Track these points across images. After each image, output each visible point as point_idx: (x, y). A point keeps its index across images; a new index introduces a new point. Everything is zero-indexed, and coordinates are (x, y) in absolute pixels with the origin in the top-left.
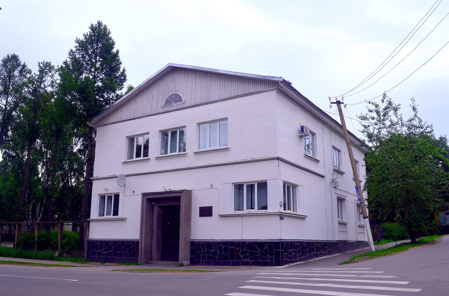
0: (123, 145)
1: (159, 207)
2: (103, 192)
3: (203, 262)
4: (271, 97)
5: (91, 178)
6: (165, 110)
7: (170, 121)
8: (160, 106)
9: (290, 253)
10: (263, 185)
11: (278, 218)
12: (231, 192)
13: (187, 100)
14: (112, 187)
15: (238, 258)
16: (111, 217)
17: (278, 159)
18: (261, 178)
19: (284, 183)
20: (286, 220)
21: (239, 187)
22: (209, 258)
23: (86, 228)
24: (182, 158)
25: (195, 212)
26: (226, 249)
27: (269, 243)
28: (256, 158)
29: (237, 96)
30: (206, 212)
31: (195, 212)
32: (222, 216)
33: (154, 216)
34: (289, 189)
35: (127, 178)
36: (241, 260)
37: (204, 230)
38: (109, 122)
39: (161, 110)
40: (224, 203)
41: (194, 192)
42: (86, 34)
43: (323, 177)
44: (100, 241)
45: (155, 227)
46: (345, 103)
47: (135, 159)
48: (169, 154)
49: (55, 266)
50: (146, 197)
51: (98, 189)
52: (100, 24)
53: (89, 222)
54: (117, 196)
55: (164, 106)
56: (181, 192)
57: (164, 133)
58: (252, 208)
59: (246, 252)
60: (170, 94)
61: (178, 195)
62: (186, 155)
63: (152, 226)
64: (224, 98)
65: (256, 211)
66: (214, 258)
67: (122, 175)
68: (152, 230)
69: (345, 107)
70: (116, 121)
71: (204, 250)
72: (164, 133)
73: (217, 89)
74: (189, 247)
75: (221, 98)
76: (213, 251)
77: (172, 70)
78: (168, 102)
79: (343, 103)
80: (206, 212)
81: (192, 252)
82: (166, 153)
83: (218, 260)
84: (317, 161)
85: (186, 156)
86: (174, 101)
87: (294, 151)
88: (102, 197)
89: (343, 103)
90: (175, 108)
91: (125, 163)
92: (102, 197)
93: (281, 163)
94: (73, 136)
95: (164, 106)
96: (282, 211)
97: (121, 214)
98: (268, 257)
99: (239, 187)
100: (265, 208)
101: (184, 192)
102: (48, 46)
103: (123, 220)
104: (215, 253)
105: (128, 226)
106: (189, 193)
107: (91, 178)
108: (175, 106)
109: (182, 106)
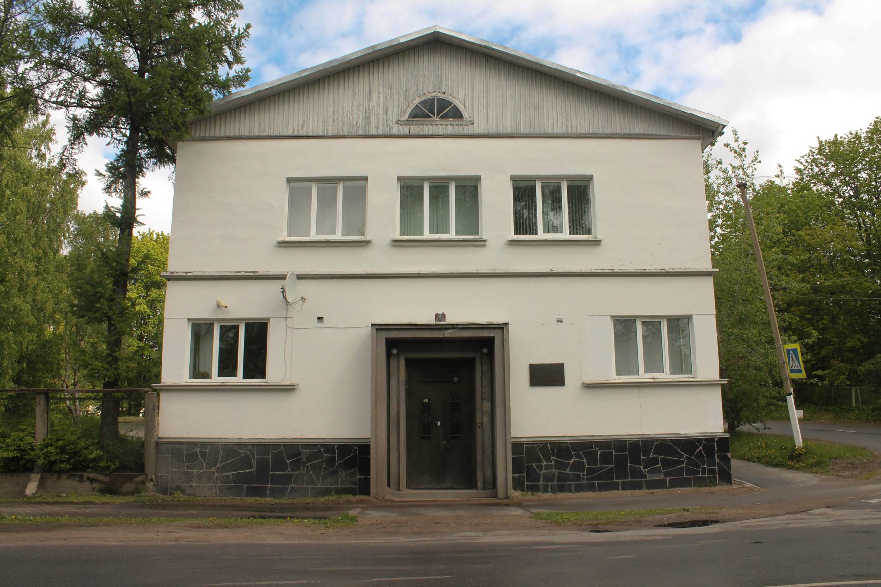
2: (204, 313)
6: (405, 130)
7: (437, 156)
15: (638, 474)
18: (255, 313)
21: (624, 326)
22: (608, 474)
23: (154, 409)
26: (606, 458)
27: (706, 440)
28: (669, 267)
29: (624, 134)
30: (547, 376)
37: (534, 416)
40: (592, 356)
41: (513, 332)
44: (212, 444)
48: (541, 235)
49: (865, 519)
59: (655, 461)
65: (238, 379)
66: (578, 477)
71: (548, 459)
72: (410, 189)
76: (572, 461)
77: (436, 44)
80: (547, 376)
81: (517, 466)
83: (588, 480)
86: (437, 111)
88: (200, 331)
91: (284, 244)
94: (158, 147)
95: (407, 123)
97: (275, 372)
98: (704, 469)
99: (624, 326)
100: (262, 374)
104: (578, 466)
108: (442, 126)
109: (459, 130)
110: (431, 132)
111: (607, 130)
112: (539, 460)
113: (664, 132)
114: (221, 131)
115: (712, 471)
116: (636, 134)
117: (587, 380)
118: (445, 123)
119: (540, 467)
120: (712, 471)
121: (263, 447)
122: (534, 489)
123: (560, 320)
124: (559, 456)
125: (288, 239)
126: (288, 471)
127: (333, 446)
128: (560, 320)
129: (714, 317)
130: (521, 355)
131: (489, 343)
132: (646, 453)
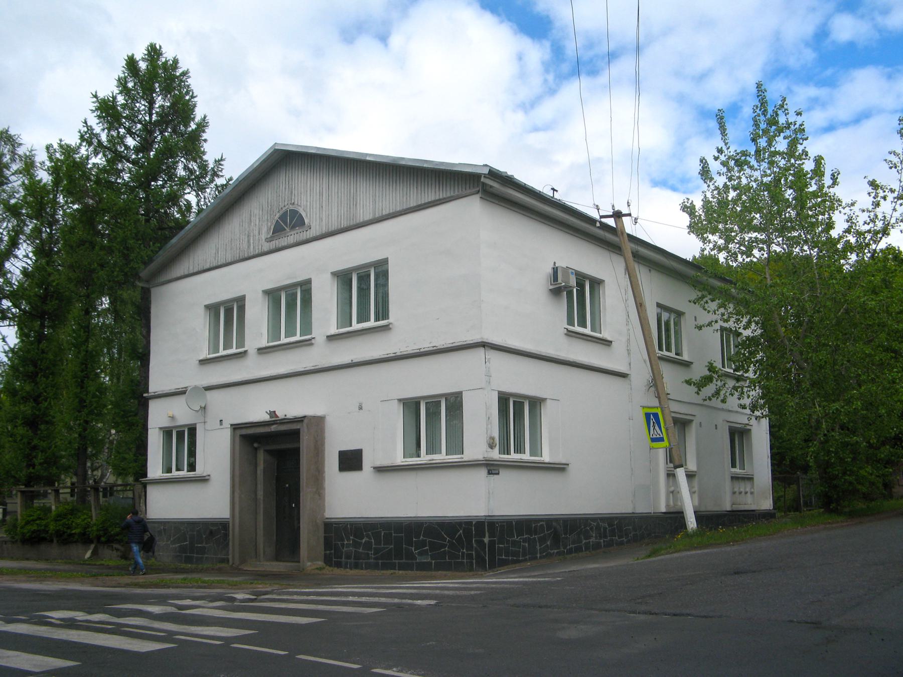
0: (200, 323)
1: (266, 451)
2: (166, 423)
3: (346, 564)
4: (471, 210)
5: (145, 395)
8: (263, 237)
9: (514, 543)
10: (455, 403)
11: (483, 472)
12: (397, 418)
13: (315, 222)
14: (178, 412)
15: (411, 556)
16: (184, 473)
17: (484, 346)
19: (503, 399)
20: (503, 473)
21: (411, 406)
23: (140, 497)
25: (332, 462)
30: (351, 461)
31: (332, 462)
32: (380, 470)
33: (259, 472)
34: (516, 411)
35: (208, 393)
36: (414, 558)
37: (348, 498)
39: (266, 247)
40: (386, 442)
43: (623, 376)
45: (260, 494)
46: (634, 215)
47: (356, 326)
50: (239, 432)
51: (158, 416)
52: (154, 52)
53: (145, 486)
54: (192, 430)
55: (269, 240)
56: (300, 420)
57: (343, 278)
59: (423, 544)
60: (281, 212)
62: (313, 341)
63: (255, 492)
64: (383, 216)
66: (368, 557)
68: (256, 500)
69: (636, 221)
70: (186, 273)
71: (348, 540)
73: (370, 197)
74: (321, 534)
75: (377, 215)
78: (278, 230)
79: (629, 215)
80: (351, 461)
81: (328, 543)
83: (375, 559)
84: (607, 343)
85: (312, 344)
86: (289, 225)
87: (542, 325)
88: (167, 433)
89: (629, 215)
90: (291, 239)
91: (203, 362)
92: (167, 433)
93: (493, 355)
96: (495, 454)
97: (200, 470)
98: (463, 553)
99: (411, 406)
101: (306, 421)
102: (57, 113)
103: (204, 480)
104: (368, 546)
105: (196, 493)
106: (318, 422)
107: (145, 395)
110: (305, 238)
111: (413, 204)
112: (343, 540)
113: (441, 195)
114: (163, 279)
115: (470, 556)
116: (425, 204)
117: (378, 464)
118: (295, 232)
119: (343, 545)
120: (470, 556)
121: (193, 524)
122: (339, 565)
123: (361, 408)
124: (355, 536)
125: (268, 345)
126: (204, 545)
127: (511, 522)
128: (361, 408)
129: (149, 427)
130: (338, 440)
131: (295, 435)
132: (418, 536)
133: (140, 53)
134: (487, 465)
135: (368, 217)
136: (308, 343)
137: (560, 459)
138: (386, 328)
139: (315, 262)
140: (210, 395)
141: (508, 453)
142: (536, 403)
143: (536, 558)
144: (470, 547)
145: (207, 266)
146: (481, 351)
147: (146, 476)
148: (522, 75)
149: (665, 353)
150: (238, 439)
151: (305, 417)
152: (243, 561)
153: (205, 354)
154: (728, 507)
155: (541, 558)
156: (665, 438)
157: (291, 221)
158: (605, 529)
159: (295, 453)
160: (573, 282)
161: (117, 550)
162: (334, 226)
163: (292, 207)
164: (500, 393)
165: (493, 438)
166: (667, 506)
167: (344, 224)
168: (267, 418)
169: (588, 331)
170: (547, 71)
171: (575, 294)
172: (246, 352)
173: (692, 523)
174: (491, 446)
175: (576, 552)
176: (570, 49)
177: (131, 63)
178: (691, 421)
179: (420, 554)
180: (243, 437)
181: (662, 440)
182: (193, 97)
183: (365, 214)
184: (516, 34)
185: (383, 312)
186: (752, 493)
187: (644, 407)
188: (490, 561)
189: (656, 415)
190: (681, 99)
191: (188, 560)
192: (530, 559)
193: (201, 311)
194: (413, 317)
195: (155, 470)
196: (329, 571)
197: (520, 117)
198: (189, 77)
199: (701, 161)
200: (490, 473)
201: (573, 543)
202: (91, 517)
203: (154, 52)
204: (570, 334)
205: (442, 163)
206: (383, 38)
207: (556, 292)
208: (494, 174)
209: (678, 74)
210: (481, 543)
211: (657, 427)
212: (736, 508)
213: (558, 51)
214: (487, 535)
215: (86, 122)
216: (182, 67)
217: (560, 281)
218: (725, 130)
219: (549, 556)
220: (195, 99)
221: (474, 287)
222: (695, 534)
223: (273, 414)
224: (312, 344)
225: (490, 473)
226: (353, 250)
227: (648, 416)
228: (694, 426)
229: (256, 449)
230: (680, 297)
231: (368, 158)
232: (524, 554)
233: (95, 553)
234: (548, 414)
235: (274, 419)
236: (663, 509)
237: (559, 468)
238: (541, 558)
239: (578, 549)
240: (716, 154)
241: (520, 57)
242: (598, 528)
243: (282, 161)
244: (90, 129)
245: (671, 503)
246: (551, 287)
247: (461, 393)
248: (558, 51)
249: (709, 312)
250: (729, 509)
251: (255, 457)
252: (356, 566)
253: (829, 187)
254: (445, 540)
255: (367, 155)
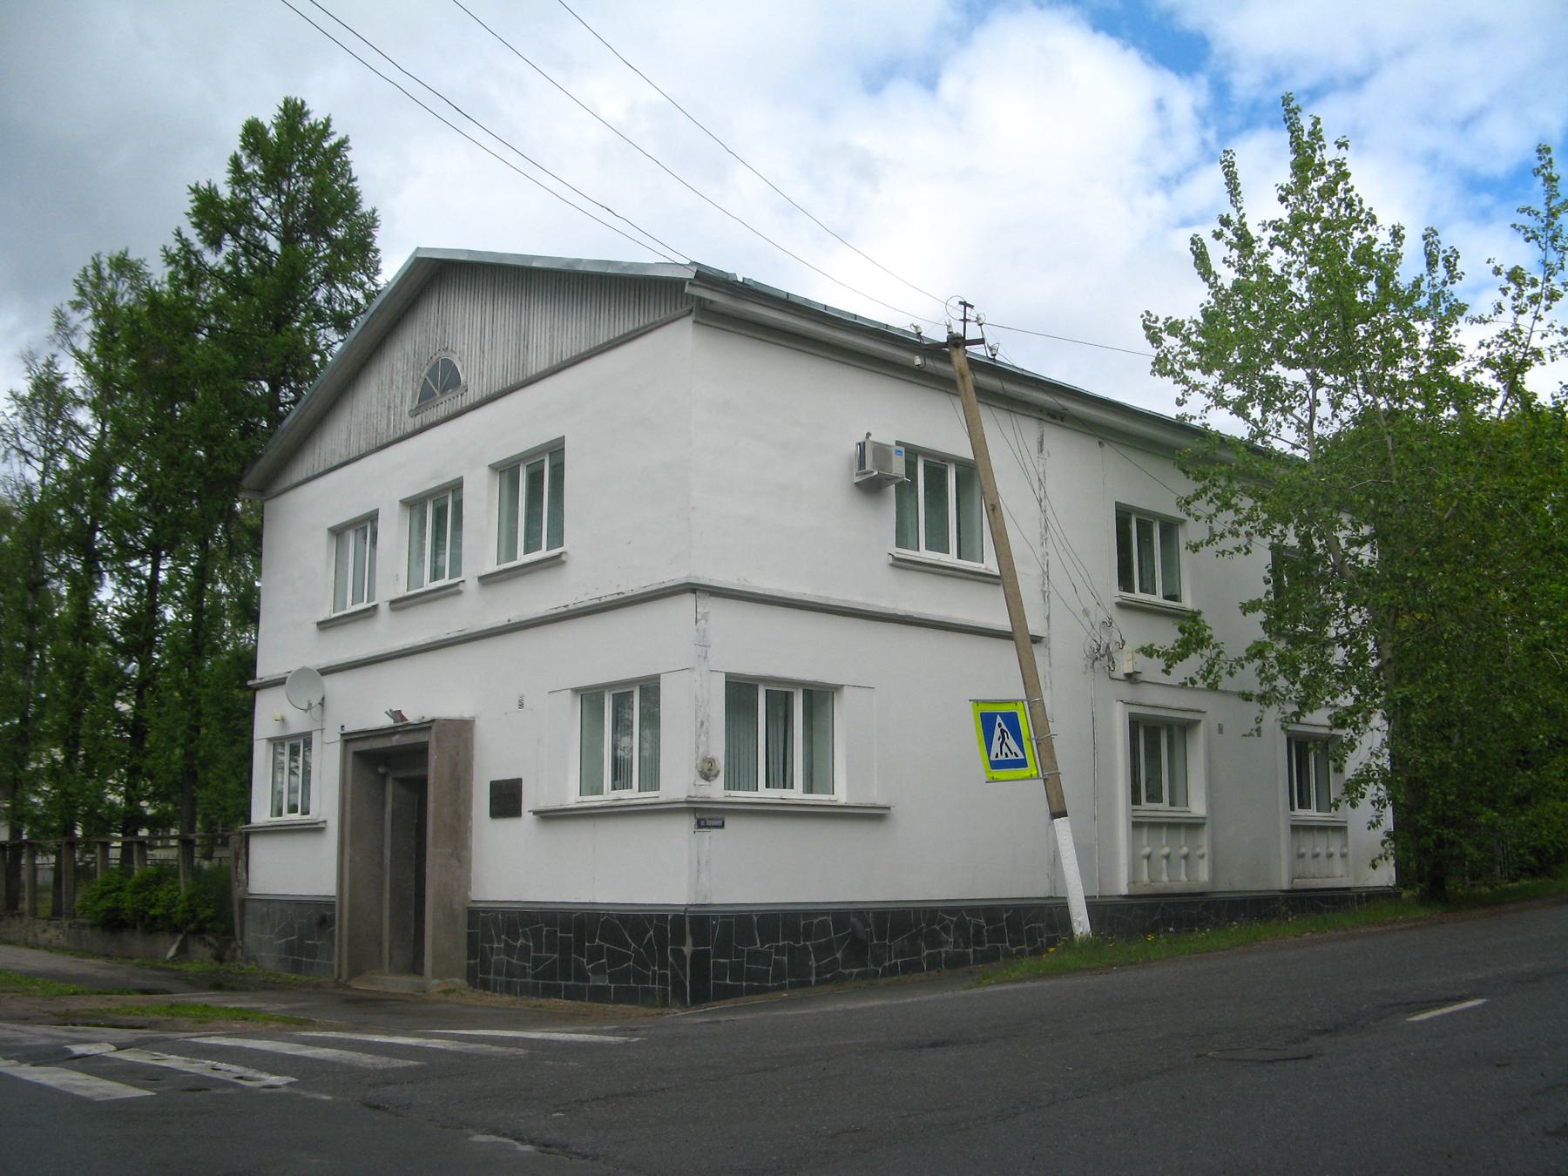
1: (395, 779)
2: (275, 732)
4: (680, 349)
5: (250, 683)
9: (754, 957)
11: (686, 824)
15: (581, 975)
21: (590, 697)
24: (451, 600)
32: (547, 816)
36: (587, 979)
37: (513, 867)
38: (287, 484)
39: (410, 424)
42: (175, 247)
52: (293, 112)
53: (246, 837)
55: (414, 413)
56: (425, 726)
58: (787, 783)
61: (420, 738)
62: (461, 587)
67: (304, 671)
68: (381, 865)
71: (499, 941)
73: (549, 330)
78: (426, 397)
80: (506, 799)
81: (474, 946)
82: (512, 556)
85: (460, 593)
86: (441, 390)
87: (853, 552)
89: (982, 341)
90: (441, 411)
91: (324, 626)
92: (276, 742)
96: (716, 790)
106: (460, 731)
107: (250, 683)
111: (603, 338)
112: (491, 942)
113: (645, 321)
115: (663, 978)
122: (485, 985)
123: (521, 705)
128: (521, 705)
130: (490, 767)
133: (268, 116)
134: (694, 811)
135: (543, 366)
136: (452, 591)
137: (873, 796)
138: (556, 562)
139: (467, 448)
140: (331, 682)
141: (599, 791)
142: (819, 697)
143: (807, 984)
144: (664, 965)
145: (335, 463)
146: (688, 600)
147: (249, 822)
148: (1166, 134)
149: (1138, 595)
150: (350, 757)
151: (433, 721)
152: (356, 970)
153: (326, 613)
154: (1282, 881)
155: (818, 983)
156: (1030, 761)
157: (443, 378)
158: (979, 928)
159: (418, 787)
160: (898, 467)
161: (210, 945)
162: (497, 388)
163: (444, 355)
164: (728, 675)
165: (711, 762)
166: (1133, 882)
167: (511, 381)
168: (388, 722)
169: (950, 559)
170: (1205, 125)
171: (927, 496)
172: (375, 607)
173: (1081, 923)
174: (707, 775)
175: (904, 972)
176: (1245, 84)
177: (253, 131)
178: (1198, 722)
179: (595, 971)
180: (360, 755)
181: (1022, 764)
182: (351, 180)
183: (538, 363)
184: (1148, 63)
185: (557, 537)
186: (1344, 856)
187: (977, 701)
188: (702, 989)
189: (1011, 720)
190: (1432, 160)
191: (296, 967)
192: (792, 986)
193: (323, 538)
194: (604, 542)
195: (261, 814)
196: (477, 998)
197: (1159, 202)
198: (348, 149)
199: (1193, 242)
200: (701, 825)
201: (901, 954)
202: (178, 889)
203: (293, 112)
204: (899, 564)
205: (631, 265)
206: (930, 83)
207: (871, 487)
208: (706, 277)
209: (1427, 119)
210: (678, 954)
211: (1011, 741)
212: (1300, 884)
213: (1221, 89)
214: (689, 940)
215: (179, 234)
216: (338, 132)
217: (868, 467)
218: (1237, 186)
219: (839, 979)
220: (355, 184)
221: (714, 483)
222: (1086, 943)
223: (397, 715)
224: (460, 593)
225: (701, 825)
226: (511, 427)
227: (988, 721)
228: (1201, 728)
229: (384, 777)
230: (1158, 489)
231: (535, 264)
232: (778, 976)
233: (183, 950)
234: (844, 717)
235: (401, 725)
236: (1124, 890)
237: (874, 815)
238: (818, 983)
239: (911, 967)
240: (1218, 227)
241: (1160, 106)
242: (961, 926)
243: (435, 275)
244: (185, 245)
245: (1145, 877)
246: (857, 479)
247: (657, 678)
248: (1221, 89)
249: (1198, 518)
250: (1286, 886)
251: (383, 789)
252: (508, 988)
253: (1444, 283)
254: (628, 946)
255: (533, 258)
